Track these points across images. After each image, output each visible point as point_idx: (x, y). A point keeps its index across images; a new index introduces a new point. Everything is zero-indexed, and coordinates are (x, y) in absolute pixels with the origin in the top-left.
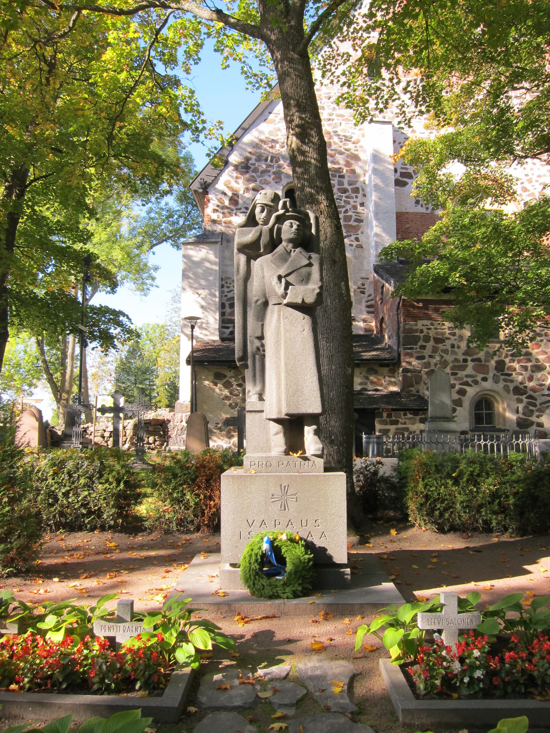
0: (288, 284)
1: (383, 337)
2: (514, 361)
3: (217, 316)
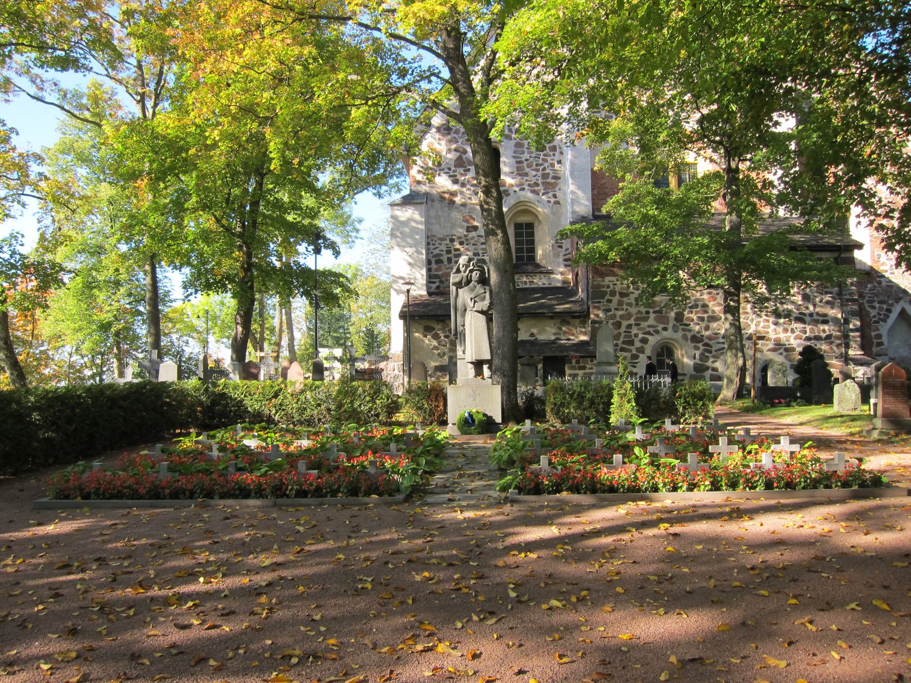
0: (475, 302)
1: (578, 289)
2: (692, 312)
3: (424, 272)
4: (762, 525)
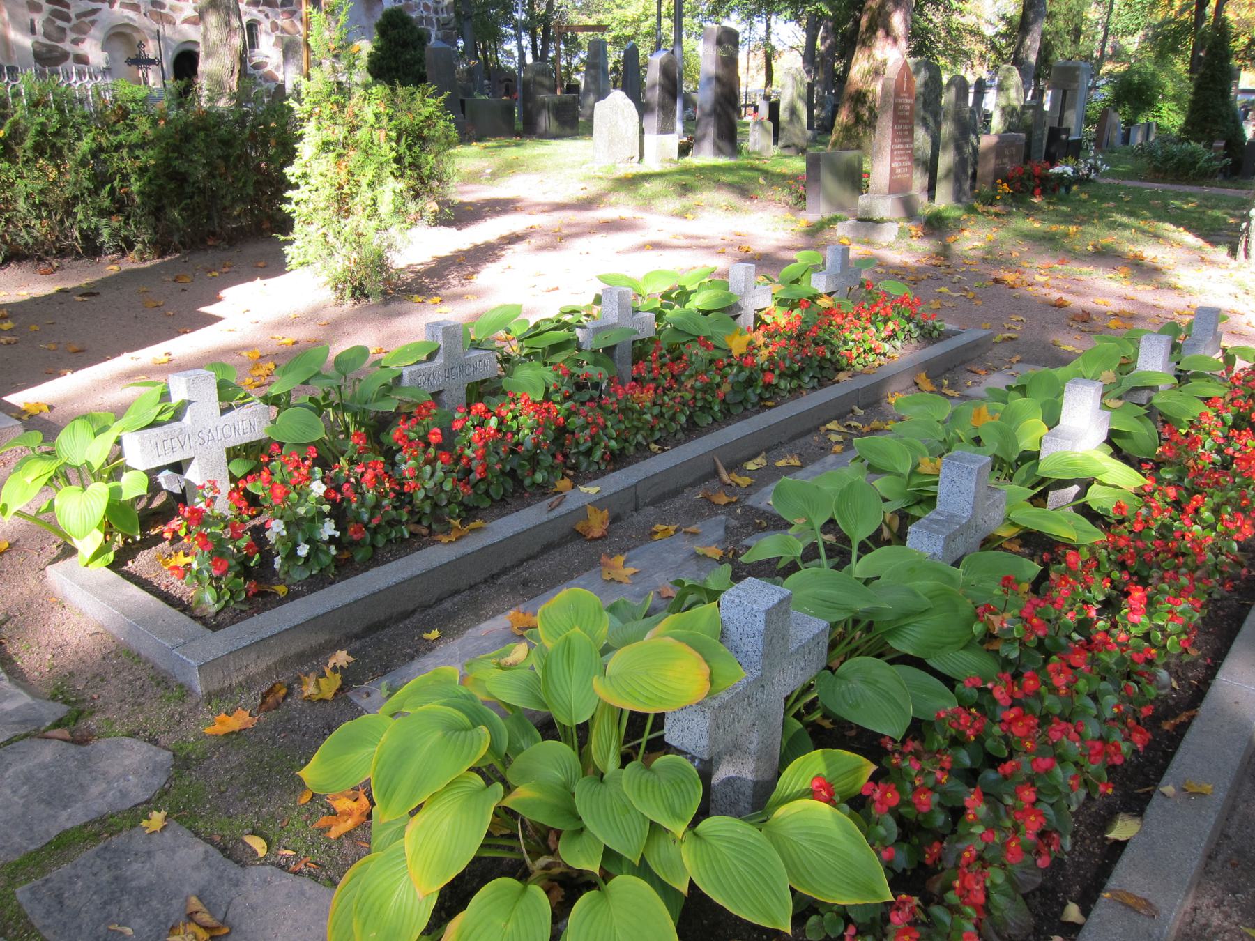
4: (977, 441)
